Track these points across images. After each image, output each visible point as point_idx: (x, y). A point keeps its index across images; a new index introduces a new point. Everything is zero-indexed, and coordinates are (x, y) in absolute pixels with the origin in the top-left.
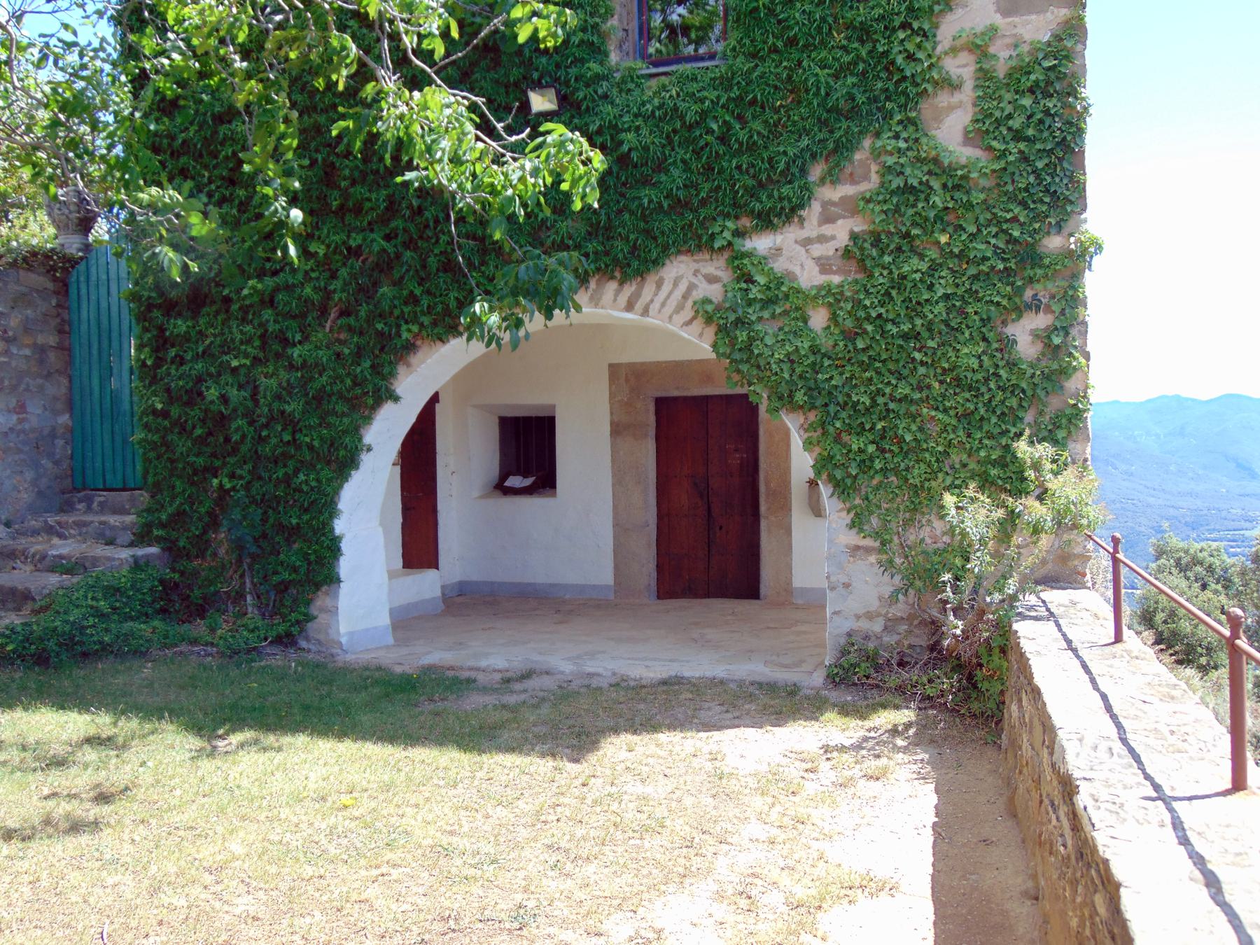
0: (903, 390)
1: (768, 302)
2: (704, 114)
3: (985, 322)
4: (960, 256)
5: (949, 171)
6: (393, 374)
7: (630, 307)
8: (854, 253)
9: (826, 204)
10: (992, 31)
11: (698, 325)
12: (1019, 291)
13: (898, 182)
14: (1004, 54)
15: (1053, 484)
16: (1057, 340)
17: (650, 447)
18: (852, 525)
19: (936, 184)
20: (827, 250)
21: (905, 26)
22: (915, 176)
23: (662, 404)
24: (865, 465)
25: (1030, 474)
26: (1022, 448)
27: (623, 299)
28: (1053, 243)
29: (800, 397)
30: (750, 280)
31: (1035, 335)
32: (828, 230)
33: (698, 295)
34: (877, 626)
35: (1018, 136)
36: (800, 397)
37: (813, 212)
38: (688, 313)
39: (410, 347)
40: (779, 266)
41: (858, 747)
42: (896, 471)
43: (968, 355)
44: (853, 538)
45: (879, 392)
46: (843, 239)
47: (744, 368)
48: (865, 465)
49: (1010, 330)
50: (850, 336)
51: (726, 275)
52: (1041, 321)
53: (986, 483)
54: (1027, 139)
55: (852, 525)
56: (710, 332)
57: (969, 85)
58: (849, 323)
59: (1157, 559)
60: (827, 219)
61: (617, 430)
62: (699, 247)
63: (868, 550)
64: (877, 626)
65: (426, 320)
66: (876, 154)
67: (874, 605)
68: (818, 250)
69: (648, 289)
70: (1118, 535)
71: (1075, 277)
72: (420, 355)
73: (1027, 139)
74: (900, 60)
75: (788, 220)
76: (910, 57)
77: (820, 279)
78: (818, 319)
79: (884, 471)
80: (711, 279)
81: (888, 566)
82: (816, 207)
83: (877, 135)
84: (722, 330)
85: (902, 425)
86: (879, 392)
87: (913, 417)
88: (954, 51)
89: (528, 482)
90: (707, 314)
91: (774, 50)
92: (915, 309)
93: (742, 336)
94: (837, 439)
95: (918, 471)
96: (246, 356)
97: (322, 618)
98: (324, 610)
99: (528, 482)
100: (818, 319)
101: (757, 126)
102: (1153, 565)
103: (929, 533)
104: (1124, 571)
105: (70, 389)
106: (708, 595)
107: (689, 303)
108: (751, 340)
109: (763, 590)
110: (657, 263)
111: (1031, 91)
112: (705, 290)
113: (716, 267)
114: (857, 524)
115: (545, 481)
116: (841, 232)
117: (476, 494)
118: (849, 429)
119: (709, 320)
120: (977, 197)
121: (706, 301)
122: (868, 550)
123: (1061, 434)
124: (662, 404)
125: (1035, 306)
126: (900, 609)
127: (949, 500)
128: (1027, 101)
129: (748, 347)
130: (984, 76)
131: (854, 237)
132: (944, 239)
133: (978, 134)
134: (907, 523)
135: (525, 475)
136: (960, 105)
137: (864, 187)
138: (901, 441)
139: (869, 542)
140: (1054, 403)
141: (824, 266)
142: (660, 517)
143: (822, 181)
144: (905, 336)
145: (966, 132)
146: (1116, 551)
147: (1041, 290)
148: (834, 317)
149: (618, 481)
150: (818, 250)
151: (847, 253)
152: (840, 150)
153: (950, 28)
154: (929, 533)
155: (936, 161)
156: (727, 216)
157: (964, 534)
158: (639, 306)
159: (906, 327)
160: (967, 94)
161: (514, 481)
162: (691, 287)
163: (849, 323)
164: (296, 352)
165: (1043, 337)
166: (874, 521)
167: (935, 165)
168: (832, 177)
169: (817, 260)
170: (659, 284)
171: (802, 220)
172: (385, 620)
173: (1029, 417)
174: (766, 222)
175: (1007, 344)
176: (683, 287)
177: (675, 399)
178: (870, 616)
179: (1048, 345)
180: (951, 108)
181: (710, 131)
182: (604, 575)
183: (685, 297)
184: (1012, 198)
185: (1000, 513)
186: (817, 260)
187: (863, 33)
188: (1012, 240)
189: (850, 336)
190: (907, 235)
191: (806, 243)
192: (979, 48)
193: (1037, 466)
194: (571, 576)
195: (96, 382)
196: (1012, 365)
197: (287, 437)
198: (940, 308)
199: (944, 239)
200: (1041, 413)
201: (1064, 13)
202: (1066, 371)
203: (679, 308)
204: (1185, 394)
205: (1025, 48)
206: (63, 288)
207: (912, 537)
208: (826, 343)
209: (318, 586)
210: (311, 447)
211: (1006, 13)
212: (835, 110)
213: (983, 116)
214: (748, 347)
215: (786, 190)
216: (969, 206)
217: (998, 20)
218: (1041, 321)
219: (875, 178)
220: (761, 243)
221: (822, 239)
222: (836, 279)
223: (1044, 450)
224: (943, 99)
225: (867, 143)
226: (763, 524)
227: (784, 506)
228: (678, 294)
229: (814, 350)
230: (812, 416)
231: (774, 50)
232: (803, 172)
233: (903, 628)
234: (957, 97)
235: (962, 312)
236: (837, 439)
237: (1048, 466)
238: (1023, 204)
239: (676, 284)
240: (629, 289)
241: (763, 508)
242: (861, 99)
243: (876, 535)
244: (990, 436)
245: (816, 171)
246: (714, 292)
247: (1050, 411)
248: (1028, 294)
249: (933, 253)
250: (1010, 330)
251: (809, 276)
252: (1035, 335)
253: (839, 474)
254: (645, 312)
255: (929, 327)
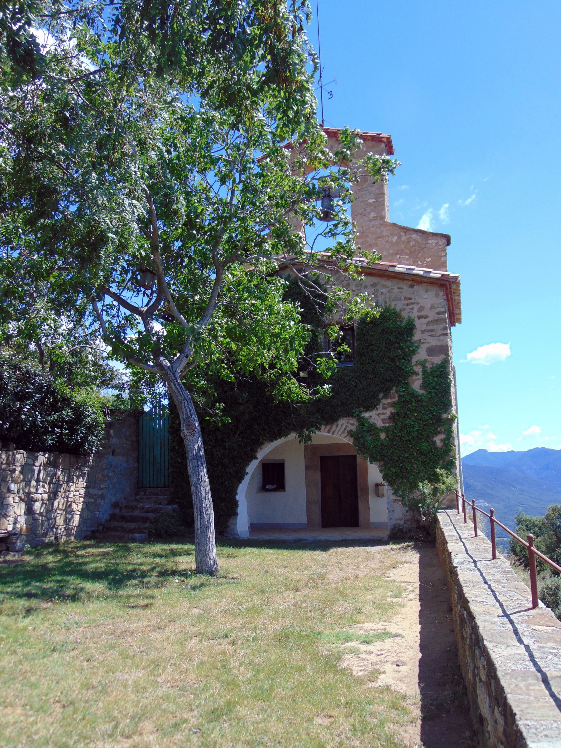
0: (407, 455)
1: (369, 431)
2: (350, 380)
3: (428, 437)
4: (420, 419)
5: (417, 397)
6: (256, 451)
7: (328, 432)
8: (392, 417)
9: (384, 404)
10: (426, 360)
11: (348, 438)
12: (436, 429)
13: (403, 399)
14: (429, 366)
15: (445, 479)
16: (446, 442)
17: (319, 473)
18: (394, 494)
19: (413, 400)
20: (384, 417)
21: (403, 358)
22: (408, 398)
23: (323, 459)
24: (397, 476)
25: (441, 477)
26: (438, 470)
27: (327, 430)
28: (444, 416)
29: (378, 457)
30: (363, 425)
31: (441, 440)
32: (384, 411)
33: (348, 429)
34: (402, 522)
35: (434, 388)
36: (378, 457)
37: (380, 406)
38: (346, 434)
39: (262, 443)
40: (371, 421)
41: (400, 549)
42: (406, 478)
43: (424, 446)
44: (394, 497)
45: (400, 456)
46: (389, 414)
47: (363, 449)
48: (397, 476)
49: (434, 439)
50: (391, 441)
51: (357, 424)
52: (443, 436)
53: (430, 481)
54: (437, 389)
55: (394, 494)
56: (352, 439)
57: (421, 374)
58: (392, 437)
59: (518, 525)
60: (384, 408)
61: (307, 468)
62: (349, 416)
63: (399, 501)
64: (402, 522)
65: (267, 435)
66: (397, 392)
67: (401, 516)
68: (382, 417)
69: (334, 427)
70: (493, 509)
71: (451, 425)
72: (265, 445)
73: (437, 389)
74: (403, 367)
75: (374, 409)
76: (406, 367)
77: (383, 425)
78: (383, 436)
79: (402, 478)
80: (352, 425)
81: (405, 505)
82: (381, 405)
83: (397, 386)
84: (355, 439)
85: (407, 465)
86: (400, 456)
87: (410, 463)
88: (416, 365)
89: (274, 487)
90: (351, 434)
91: (369, 363)
92: (408, 433)
93: (362, 441)
94: (389, 469)
95: (411, 478)
96: (210, 445)
97: (232, 526)
98: (233, 524)
99: (274, 487)
100: (383, 436)
101: (365, 383)
102: (517, 528)
103: (416, 494)
104: (466, 504)
105: (138, 455)
106: (340, 526)
107: (346, 431)
108: (364, 442)
109: (360, 524)
110: (337, 420)
111: (437, 377)
112: (350, 427)
113: (353, 421)
114: (395, 493)
115: (280, 486)
116: (388, 412)
117: (255, 491)
118: (392, 466)
119: (352, 436)
120: (425, 404)
121: (351, 431)
122: (399, 501)
123: (449, 467)
124: (323, 459)
125: (441, 432)
126: (408, 517)
127: (420, 484)
128: (436, 379)
129: (363, 444)
130: (424, 371)
131: (392, 413)
132: (416, 415)
133: (423, 387)
134: (410, 492)
135: (273, 484)
136: (418, 379)
137: (394, 400)
138: (407, 469)
139: (399, 498)
140: (447, 458)
141: (384, 421)
142: (322, 498)
143: (383, 398)
144: (407, 441)
145: (420, 386)
146: (492, 516)
147: (442, 429)
148: (387, 436)
149: (308, 486)
150: (382, 417)
151: (390, 418)
152: (388, 390)
153: (415, 359)
154: (416, 494)
155: (413, 393)
156: (357, 407)
157: (424, 493)
158: (331, 432)
159: (407, 439)
160: (420, 376)
161: (268, 487)
162: (347, 426)
163: (392, 437)
164: (227, 444)
165: (443, 441)
166: (400, 492)
167: (413, 394)
168: (385, 397)
169: (382, 420)
170: (337, 426)
171: (377, 409)
172: (247, 529)
173: (441, 462)
174: (367, 409)
175: (434, 443)
176: (344, 426)
177: (327, 457)
178: (400, 519)
179: (444, 443)
180: (416, 380)
181: (351, 384)
182: (303, 519)
183: (345, 429)
184: (433, 404)
185: (433, 487)
186: (382, 420)
187: (393, 360)
188: (433, 415)
189: (391, 441)
190: (406, 413)
191: (379, 415)
192: (422, 364)
193: (442, 475)
194: (290, 520)
195: (148, 452)
196: (436, 448)
197: (223, 470)
198: (416, 434)
199: (416, 415)
200: (444, 461)
201: (444, 356)
202: (450, 450)
203: (343, 433)
204: (548, 447)
205: (435, 365)
206: (138, 421)
207: (411, 496)
208: (385, 443)
209: (230, 517)
210: (230, 473)
211: (429, 356)
212: (386, 380)
213: (424, 382)
214: (363, 444)
215: (373, 401)
216: (422, 406)
217: (427, 357)
218: (443, 436)
219: (397, 398)
220: (366, 415)
221: (383, 414)
222: (387, 425)
223: (443, 471)
224: (414, 377)
225: (394, 388)
226: (359, 500)
227: (367, 494)
228: (343, 428)
229: (382, 444)
230: (382, 463)
231: (369, 363)
232: (377, 396)
233: (409, 522)
234: (418, 377)
235: (421, 434)
236: (389, 469)
237: (445, 475)
238: (436, 405)
239: (342, 425)
240: (328, 427)
241: (359, 494)
242: (393, 377)
243: (401, 496)
244: (431, 468)
245: (381, 395)
246: (354, 428)
247: (446, 461)
248: (439, 429)
249: (413, 418)
250: (434, 439)
251: (380, 424)
252: (441, 440)
253: (390, 479)
254: (333, 433)
255: (413, 438)
